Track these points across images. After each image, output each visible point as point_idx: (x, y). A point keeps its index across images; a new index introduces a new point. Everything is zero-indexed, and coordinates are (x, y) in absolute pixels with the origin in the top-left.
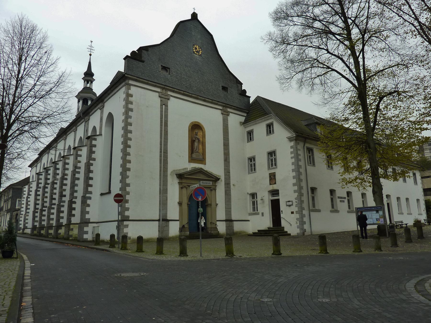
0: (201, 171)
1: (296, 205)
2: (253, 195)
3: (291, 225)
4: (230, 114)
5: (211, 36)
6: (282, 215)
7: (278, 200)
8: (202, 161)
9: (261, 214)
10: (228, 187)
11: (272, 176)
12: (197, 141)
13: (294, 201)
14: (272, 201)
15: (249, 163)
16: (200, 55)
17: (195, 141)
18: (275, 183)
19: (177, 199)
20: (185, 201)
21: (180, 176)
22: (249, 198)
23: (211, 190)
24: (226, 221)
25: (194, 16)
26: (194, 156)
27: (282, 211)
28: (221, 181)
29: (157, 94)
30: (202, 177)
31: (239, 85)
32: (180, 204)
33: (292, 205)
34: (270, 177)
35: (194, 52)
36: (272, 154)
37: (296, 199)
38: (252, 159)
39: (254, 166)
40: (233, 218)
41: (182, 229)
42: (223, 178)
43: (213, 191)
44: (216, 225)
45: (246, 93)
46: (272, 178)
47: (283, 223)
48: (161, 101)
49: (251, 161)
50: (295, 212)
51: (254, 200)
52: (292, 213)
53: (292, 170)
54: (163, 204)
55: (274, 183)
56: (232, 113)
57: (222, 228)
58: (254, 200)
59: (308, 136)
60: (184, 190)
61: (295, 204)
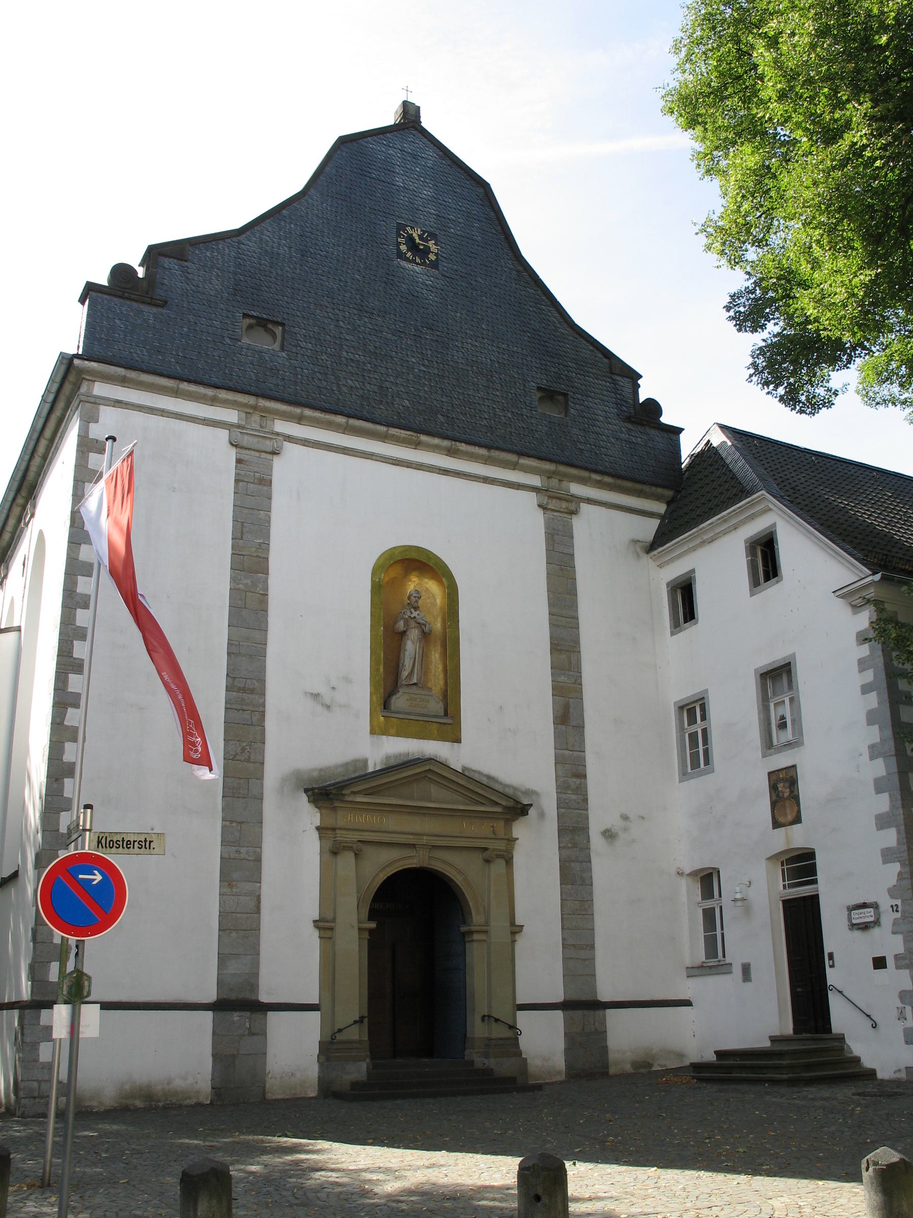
0: (426, 770)
1: (895, 922)
2: (707, 880)
3: (875, 1026)
4: (584, 507)
5: (485, 187)
6: (832, 976)
7: (814, 900)
8: (447, 723)
9: (737, 970)
10: (575, 845)
11: (780, 786)
12: (414, 634)
13: (885, 902)
14: (788, 905)
15: (681, 729)
16: (434, 265)
17: (404, 633)
18: (797, 820)
19: (310, 906)
20: (352, 919)
21: (326, 792)
22: (688, 894)
23: (487, 861)
24: (565, 1006)
25: (410, 115)
26: (400, 701)
27: (831, 956)
28: (542, 815)
29: (224, 434)
30: (439, 797)
31: (624, 383)
32: (325, 926)
33: (877, 923)
34: (773, 788)
35: (400, 255)
36: (777, 677)
37: (892, 892)
38: (694, 710)
39: (705, 741)
40: (605, 994)
41: (330, 1049)
42: (549, 802)
43: (499, 866)
44: (513, 1027)
45: (661, 414)
46: (784, 791)
47: (841, 1017)
48: (239, 461)
49: (692, 721)
50: (890, 962)
51: (708, 904)
52: (879, 963)
53: (872, 747)
54: (240, 927)
55: (790, 818)
56: (589, 501)
57: (543, 1041)
58: (708, 904)
59: (255, 408)
60: (347, 861)
61: (888, 918)
